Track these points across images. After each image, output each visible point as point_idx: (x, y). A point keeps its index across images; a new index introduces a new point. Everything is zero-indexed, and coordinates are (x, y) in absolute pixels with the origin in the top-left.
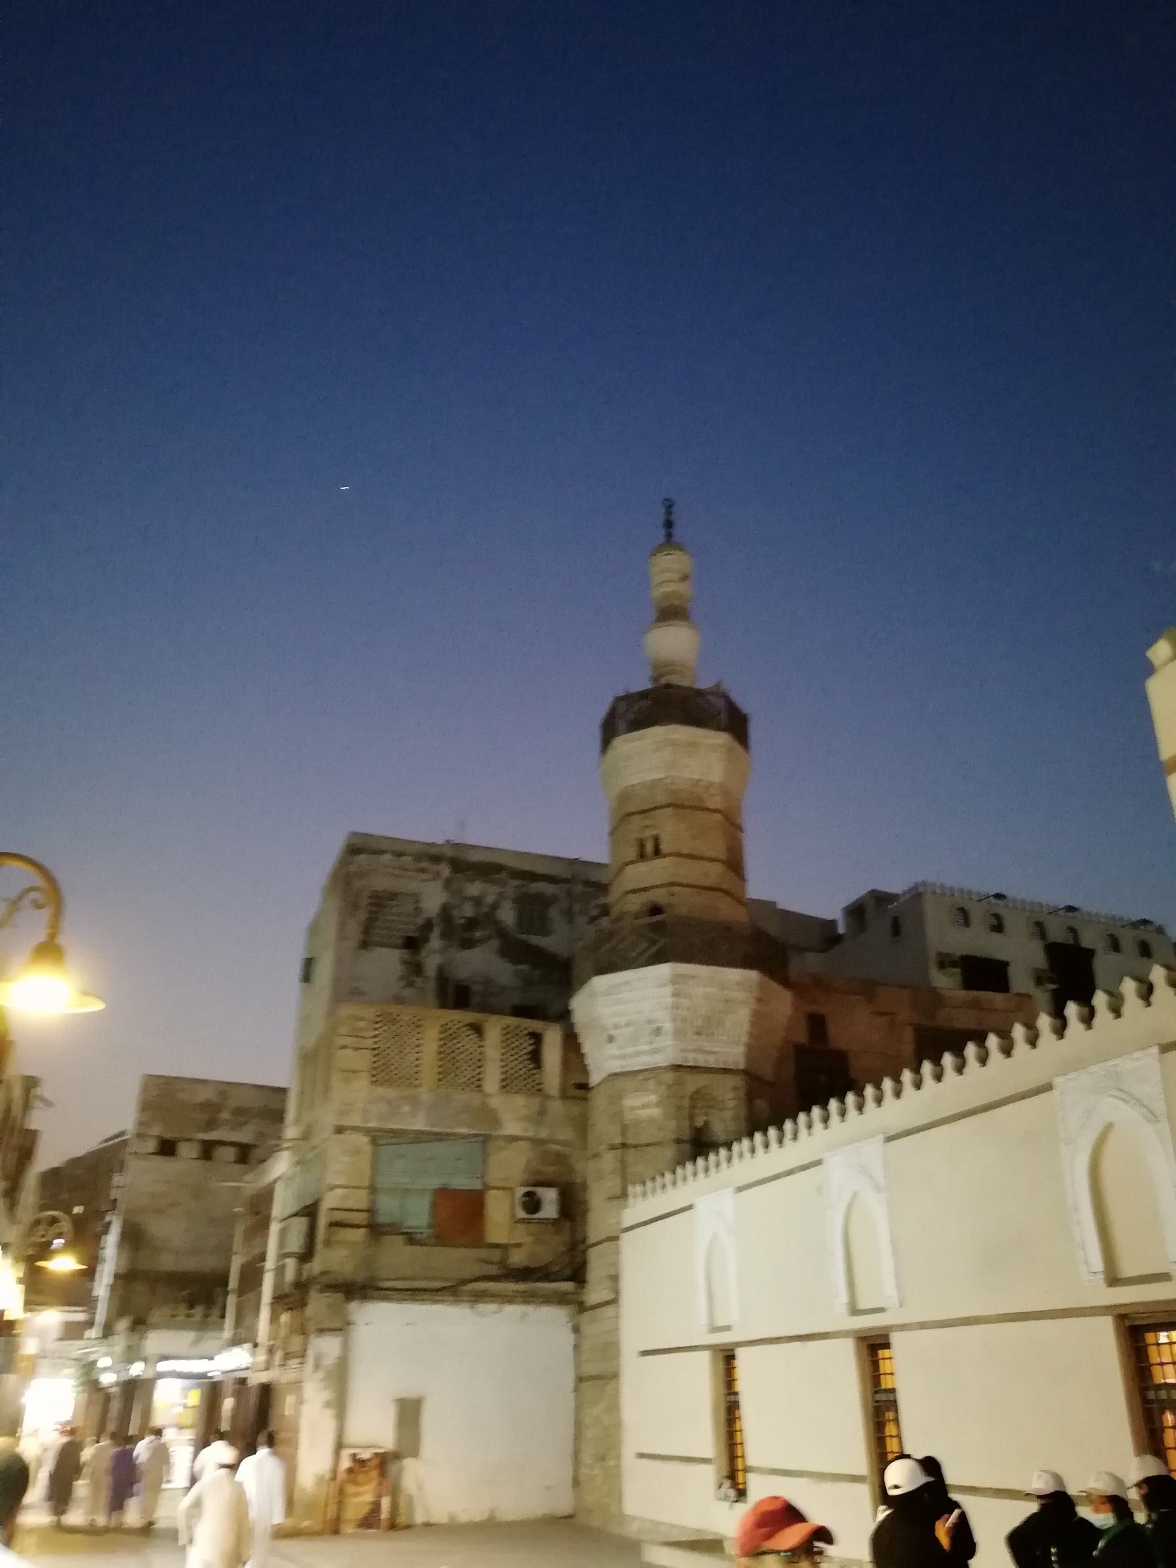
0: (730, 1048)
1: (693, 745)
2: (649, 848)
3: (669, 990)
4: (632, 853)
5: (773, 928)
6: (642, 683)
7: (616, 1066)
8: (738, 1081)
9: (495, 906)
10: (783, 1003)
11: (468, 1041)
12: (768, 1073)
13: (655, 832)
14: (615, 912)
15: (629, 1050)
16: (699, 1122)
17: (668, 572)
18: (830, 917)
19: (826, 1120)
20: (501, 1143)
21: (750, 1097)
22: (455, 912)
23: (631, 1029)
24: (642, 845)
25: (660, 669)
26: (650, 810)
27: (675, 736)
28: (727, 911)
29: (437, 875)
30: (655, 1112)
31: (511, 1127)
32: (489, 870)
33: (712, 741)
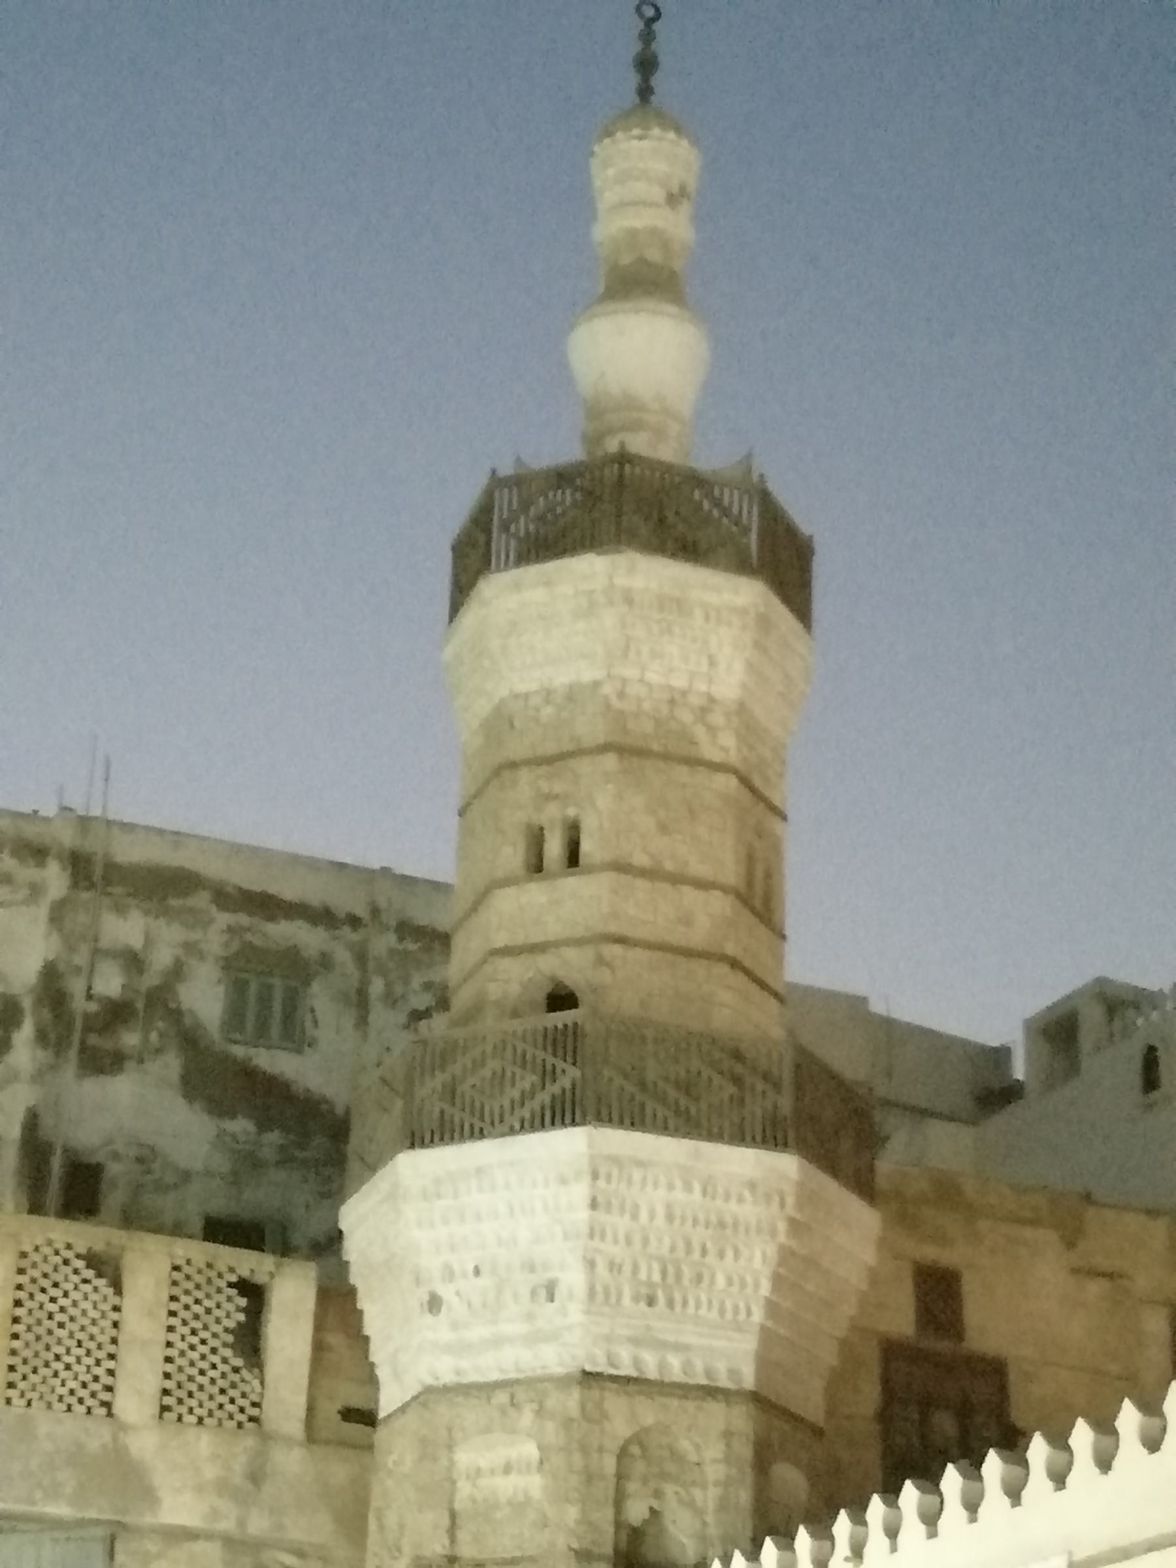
0: (721, 1336)
1: (674, 606)
2: (554, 848)
3: (580, 1191)
4: (513, 856)
5: (848, 1060)
6: (561, 448)
7: (445, 1370)
8: (741, 1419)
9: (177, 972)
10: (857, 1234)
11: (87, 1297)
12: (810, 1402)
13: (571, 812)
14: (460, 1000)
15: (478, 1332)
16: (636, 1512)
17: (640, 179)
18: (993, 1041)
19: (931, 1519)
20: (152, 1546)
21: (763, 1460)
22: (76, 986)
23: (485, 1281)
24: (536, 839)
25: (598, 414)
26: (562, 757)
27: (638, 582)
28: (731, 1009)
29: (36, 891)
30: (534, 1484)
31: (179, 1508)
32: (162, 886)
33: (727, 597)
